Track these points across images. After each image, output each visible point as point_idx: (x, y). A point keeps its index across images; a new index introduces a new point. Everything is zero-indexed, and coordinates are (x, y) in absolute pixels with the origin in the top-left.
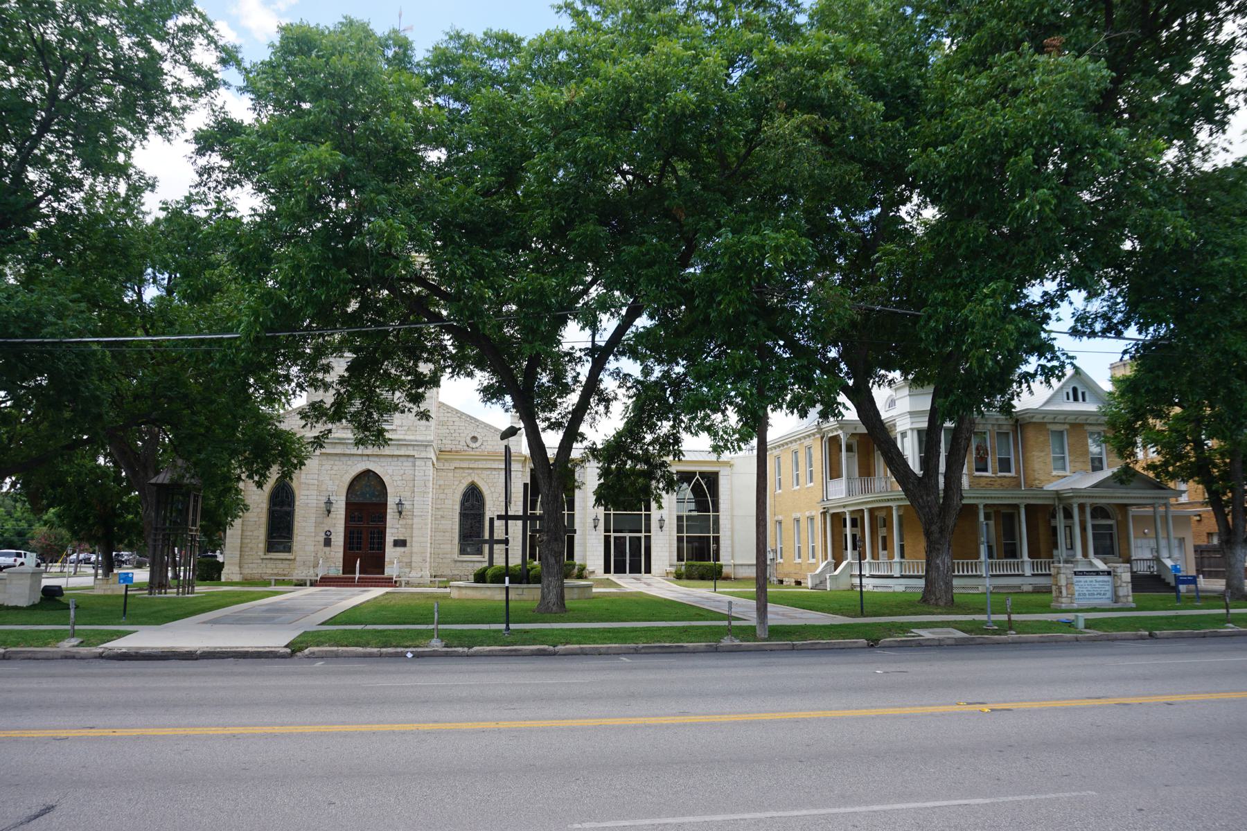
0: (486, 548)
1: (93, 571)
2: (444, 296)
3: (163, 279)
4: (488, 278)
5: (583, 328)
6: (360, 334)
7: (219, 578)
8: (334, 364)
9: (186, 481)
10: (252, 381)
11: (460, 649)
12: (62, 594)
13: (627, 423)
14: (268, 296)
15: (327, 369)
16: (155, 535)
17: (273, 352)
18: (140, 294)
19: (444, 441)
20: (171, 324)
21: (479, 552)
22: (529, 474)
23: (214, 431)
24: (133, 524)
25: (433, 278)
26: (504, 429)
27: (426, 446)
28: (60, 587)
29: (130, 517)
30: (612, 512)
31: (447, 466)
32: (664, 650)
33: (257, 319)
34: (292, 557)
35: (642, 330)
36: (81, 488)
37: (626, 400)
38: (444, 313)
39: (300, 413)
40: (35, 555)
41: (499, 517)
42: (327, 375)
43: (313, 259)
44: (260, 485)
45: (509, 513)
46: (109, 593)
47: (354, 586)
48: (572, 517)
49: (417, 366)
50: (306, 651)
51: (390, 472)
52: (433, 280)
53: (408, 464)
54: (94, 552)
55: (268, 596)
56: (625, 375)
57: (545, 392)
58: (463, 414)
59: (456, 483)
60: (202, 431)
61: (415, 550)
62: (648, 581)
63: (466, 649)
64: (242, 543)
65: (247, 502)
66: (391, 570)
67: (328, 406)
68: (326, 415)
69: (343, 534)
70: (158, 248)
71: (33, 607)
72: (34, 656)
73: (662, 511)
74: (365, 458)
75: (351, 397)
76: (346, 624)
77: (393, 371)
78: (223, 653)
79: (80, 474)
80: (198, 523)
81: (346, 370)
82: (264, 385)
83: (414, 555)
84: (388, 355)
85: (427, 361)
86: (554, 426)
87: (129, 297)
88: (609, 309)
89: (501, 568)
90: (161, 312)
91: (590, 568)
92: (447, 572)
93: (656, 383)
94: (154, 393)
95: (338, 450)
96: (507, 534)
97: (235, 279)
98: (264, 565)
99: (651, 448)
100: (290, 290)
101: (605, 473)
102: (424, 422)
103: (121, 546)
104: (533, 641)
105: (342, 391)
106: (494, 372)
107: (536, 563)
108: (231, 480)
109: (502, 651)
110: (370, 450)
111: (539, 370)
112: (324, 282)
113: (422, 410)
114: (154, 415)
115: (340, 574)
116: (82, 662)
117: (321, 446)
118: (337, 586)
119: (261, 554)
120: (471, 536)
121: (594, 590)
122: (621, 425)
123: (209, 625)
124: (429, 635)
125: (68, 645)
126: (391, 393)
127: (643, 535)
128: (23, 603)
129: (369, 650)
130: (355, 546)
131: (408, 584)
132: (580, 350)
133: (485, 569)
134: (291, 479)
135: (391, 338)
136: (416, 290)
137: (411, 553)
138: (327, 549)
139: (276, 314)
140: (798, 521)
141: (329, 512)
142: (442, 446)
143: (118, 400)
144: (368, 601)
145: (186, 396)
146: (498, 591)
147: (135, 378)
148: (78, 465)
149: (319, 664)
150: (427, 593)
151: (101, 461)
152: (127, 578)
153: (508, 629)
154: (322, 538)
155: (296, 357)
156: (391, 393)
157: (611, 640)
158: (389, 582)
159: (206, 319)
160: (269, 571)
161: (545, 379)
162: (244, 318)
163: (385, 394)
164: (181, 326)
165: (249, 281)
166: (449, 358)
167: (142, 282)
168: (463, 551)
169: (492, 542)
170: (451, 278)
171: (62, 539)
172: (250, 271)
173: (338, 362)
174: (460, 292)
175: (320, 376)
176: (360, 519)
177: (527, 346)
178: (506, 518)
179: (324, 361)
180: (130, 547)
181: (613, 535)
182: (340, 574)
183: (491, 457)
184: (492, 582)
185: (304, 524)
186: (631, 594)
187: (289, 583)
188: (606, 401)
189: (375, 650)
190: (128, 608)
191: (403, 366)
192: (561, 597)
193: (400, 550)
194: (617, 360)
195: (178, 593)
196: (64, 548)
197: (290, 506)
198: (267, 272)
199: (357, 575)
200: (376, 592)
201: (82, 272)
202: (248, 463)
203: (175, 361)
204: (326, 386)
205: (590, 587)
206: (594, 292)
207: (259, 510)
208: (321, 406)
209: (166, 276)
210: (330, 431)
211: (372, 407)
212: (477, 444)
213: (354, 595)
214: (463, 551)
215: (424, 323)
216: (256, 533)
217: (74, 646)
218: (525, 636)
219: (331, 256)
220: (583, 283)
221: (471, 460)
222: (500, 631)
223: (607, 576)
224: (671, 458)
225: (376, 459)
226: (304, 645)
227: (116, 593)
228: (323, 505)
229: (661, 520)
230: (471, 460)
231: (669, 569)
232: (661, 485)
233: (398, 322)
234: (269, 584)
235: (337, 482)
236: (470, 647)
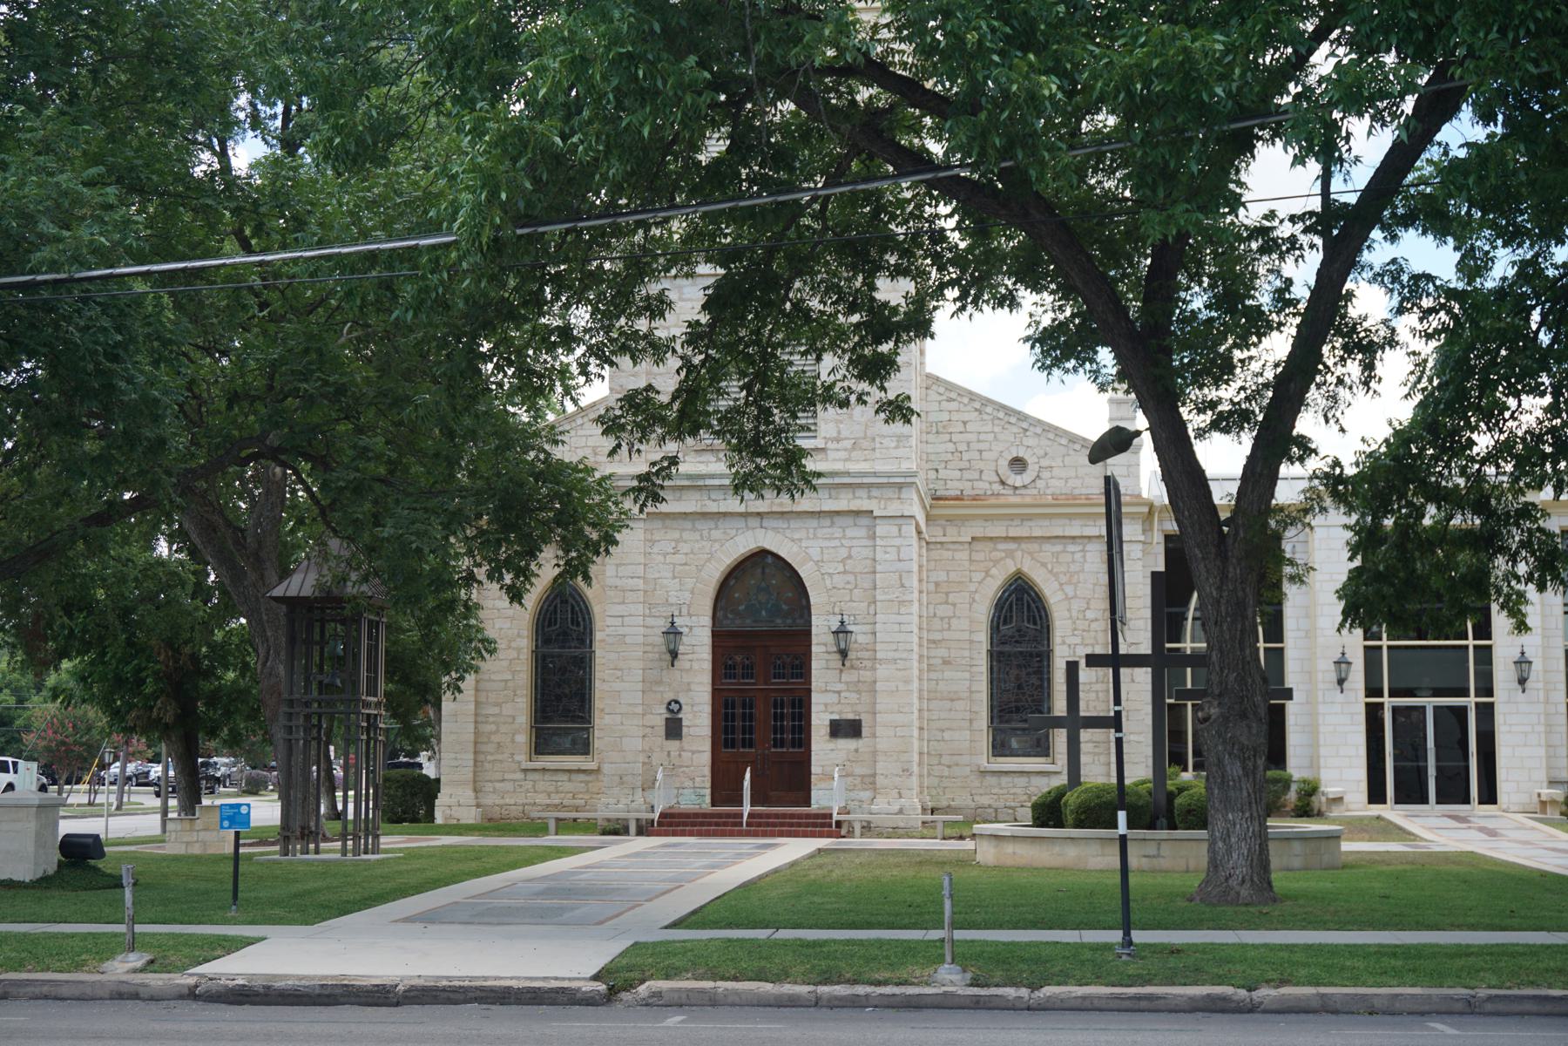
0: (1060, 738)
1: (157, 802)
2: (936, 105)
3: (274, 117)
4: (1046, 47)
5: (1299, 160)
6: (733, 216)
7: (430, 817)
8: (672, 296)
9: (350, 589)
10: (486, 347)
11: (1010, 992)
12: (102, 855)
13: (1421, 405)
14: (515, 140)
15: (658, 307)
16: (290, 716)
17: (534, 274)
18: (223, 155)
19: (942, 474)
20: (299, 223)
21: (1042, 748)
22: (1161, 549)
23: (406, 470)
24: (238, 694)
25: (904, 55)
26: (1094, 436)
27: (900, 486)
28: (96, 837)
29: (231, 675)
30: (1385, 643)
31: (952, 534)
32: (1548, 1008)
33: (494, 194)
34: (593, 766)
35: (1462, 153)
36: (125, 613)
37: (1418, 345)
38: (936, 148)
39: (600, 420)
40: (34, 765)
41: (1093, 660)
42: (658, 323)
43: (616, 40)
44: (515, 595)
45: (1123, 650)
46: (196, 850)
47: (741, 834)
48: (1277, 656)
49: (873, 288)
50: (643, 990)
51: (815, 553)
52: (904, 65)
53: (857, 532)
54: (156, 759)
55: (544, 859)
56: (1416, 278)
57: (1203, 336)
58: (987, 402)
59: (978, 577)
60: (382, 470)
61: (882, 744)
62: (1490, 824)
63: (1024, 992)
64: (477, 733)
65: (490, 633)
66: (825, 796)
67: (664, 398)
68: (662, 421)
69: (707, 709)
70: (262, 44)
71: (44, 883)
72: (54, 991)
73: (1525, 639)
74: (754, 522)
75: (716, 372)
76: (729, 926)
77: (815, 304)
78: (455, 990)
79: (122, 580)
80: (382, 686)
81: (704, 307)
82: (509, 354)
83: (880, 758)
84: (801, 265)
85: (897, 272)
86: (1227, 422)
87: (204, 164)
88: (1371, 101)
89: (1102, 790)
90: (275, 195)
91: (1330, 788)
92: (962, 799)
93: (1501, 293)
94: (270, 388)
95: (690, 504)
96: (1117, 701)
97: (438, 103)
98: (529, 785)
99: (1490, 470)
100: (567, 119)
101: (1366, 541)
102: (898, 427)
103: (212, 744)
104: (1195, 976)
105: (697, 360)
106: (1066, 292)
107: (1187, 776)
108: (452, 584)
109: (1118, 997)
110: (771, 501)
112: (646, 95)
113: (891, 396)
114: (273, 439)
115: (706, 804)
116: (153, 1006)
117: (657, 498)
118: (700, 834)
119: (522, 757)
120: (1018, 710)
121: (1346, 846)
122: (1405, 412)
123: (419, 926)
124: (931, 955)
125: (122, 968)
126: (811, 358)
127: (1471, 701)
128: (24, 872)
129: (788, 988)
130: (788, 736)
131: (868, 829)
132: (1293, 219)
133: (1060, 793)
134: (587, 578)
135: (806, 221)
136: (864, 94)
137: (874, 753)
138: (673, 745)
139: (536, 181)
140: (923, 823)
141: (674, 654)
142: (939, 485)
143: (193, 412)
144: (776, 871)
145: (341, 390)
146: (1094, 849)
147: (224, 353)
148: (117, 559)
149: (675, 1020)
150: (918, 853)
151: (163, 548)
152: (236, 817)
153: (1128, 942)
154: (659, 718)
155: (578, 287)
156: (811, 358)
157: (1399, 977)
158: (822, 824)
159: (373, 204)
160: (542, 799)
161: (1197, 300)
162: (465, 196)
163: (797, 361)
164: (320, 225)
165: (470, 105)
166: (952, 262)
167: (226, 129)
168: (1000, 748)
169: (1075, 722)
170: (955, 57)
171: (89, 729)
172: (470, 81)
173: (680, 288)
174: (976, 88)
175: (642, 325)
176: (748, 671)
177: (1155, 216)
178: (1115, 661)
179: (653, 289)
180: (234, 744)
181: (1388, 701)
182: (706, 804)
183: (1065, 507)
184: (1079, 824)
185: (617, 686)
186: (1446, 857)
187: (588, 827)
188: (1366, 349)
189: (803, 989)
190: (241, 886)
191: (838, 290)
192: (1262, 865)
193: (846, 745)
194: (1394, 238)
195: (344, 852)
196: (93, 749)
197: (582, 642)
198: (506, 83)
199: (747, 809)
200: (792, 850)
201: (102, 115)
202: (485, 544)
203: (312, 308)
204: (659, 349)
205: (1334, 838)
206: (1323, 61)
207: (514, 654)
208: (648, 400)
209: (280, 108)
210: (674, 461)
211: (770, 396)
212: (1026, 478)
213: (740, 856)
214: (1000, 748)
215: (887, 177)
216: (507, 709)
217: (135, 971)
218: (1173, 962)
219: (657, 28)
220: (1295, 38)
221: (1011, 517)
222: (1107, 947)
223: (1376, 810)
224: (1548, 493)
225: (781, 524)
226: (636, 974)
227: (210, 851)
228: (660, 640)
229: (1523, 663)
230: (1011, 517)
231: (1547, 792)
232: (1522, 569)
233: (820, 181)
234: (540, 829)
235: (690, 583)
236: (1034, 987)
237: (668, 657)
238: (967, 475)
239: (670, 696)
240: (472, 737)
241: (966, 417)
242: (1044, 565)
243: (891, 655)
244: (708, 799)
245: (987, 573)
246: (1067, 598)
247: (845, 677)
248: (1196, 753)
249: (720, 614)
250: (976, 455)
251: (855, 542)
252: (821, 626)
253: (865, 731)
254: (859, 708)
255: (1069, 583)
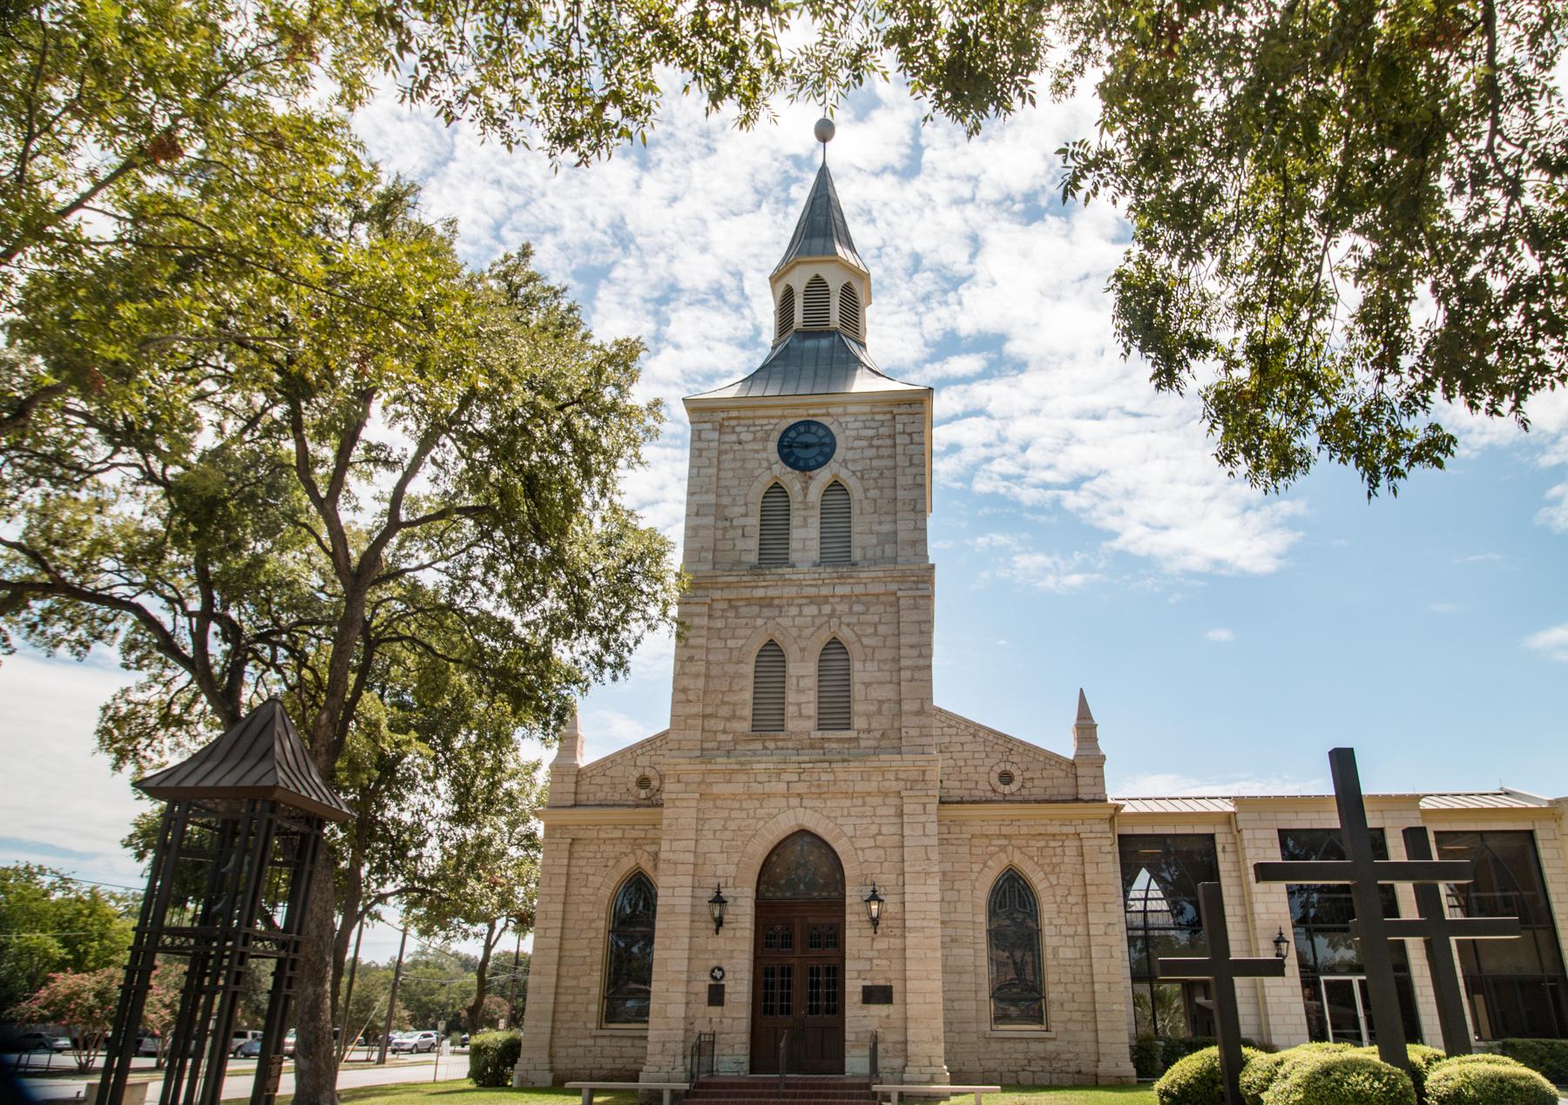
59: (977, 867)
61: (912, 1011)
111: (1449, 137)
154: (702, 985)
207: (592, 934)
216: (584, 982)
237: (714, 926)
238: (965, 785)
239: (714, 963)
240: (551, 1007)
241: (963, 739)
242: (1031, 858)
243: (919, 923)
244: (746, 1067)
245: (985, 864)
246: (1052, 886)
247: (877, 945)
248: (1370, 1025)
249: (762, 888)
250: (972, 769)
251: (885, 820)
252: (853, 895)
253: (896, 997)
254: (891, 975)
255: (1053, 872)
